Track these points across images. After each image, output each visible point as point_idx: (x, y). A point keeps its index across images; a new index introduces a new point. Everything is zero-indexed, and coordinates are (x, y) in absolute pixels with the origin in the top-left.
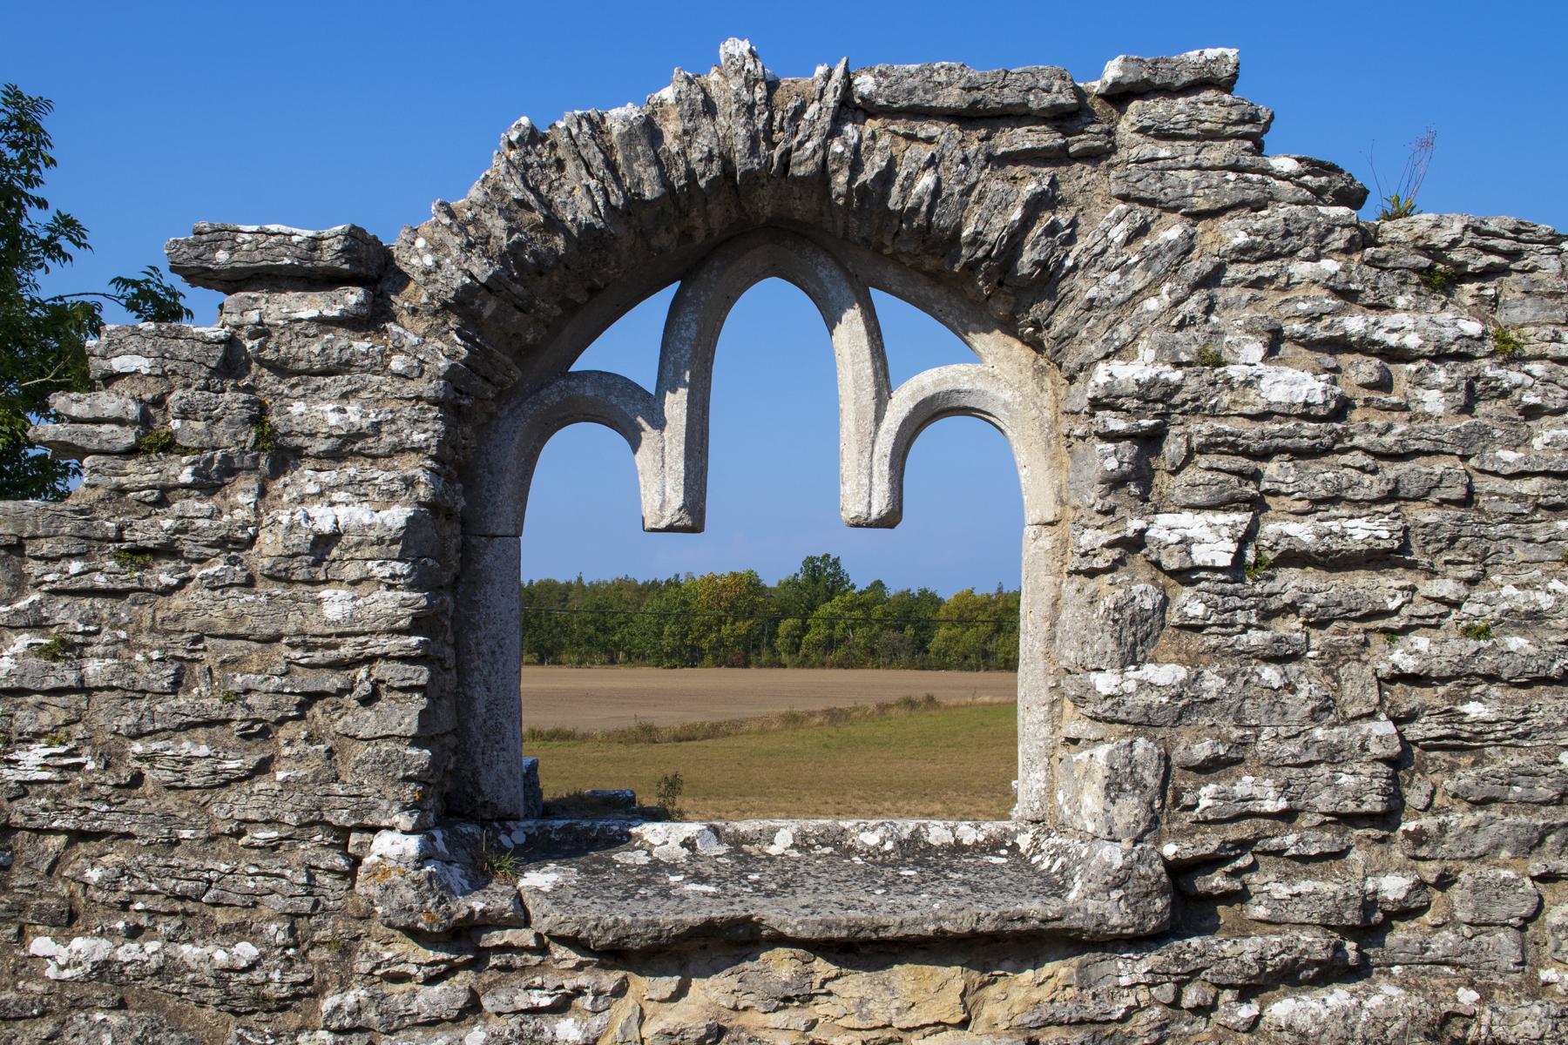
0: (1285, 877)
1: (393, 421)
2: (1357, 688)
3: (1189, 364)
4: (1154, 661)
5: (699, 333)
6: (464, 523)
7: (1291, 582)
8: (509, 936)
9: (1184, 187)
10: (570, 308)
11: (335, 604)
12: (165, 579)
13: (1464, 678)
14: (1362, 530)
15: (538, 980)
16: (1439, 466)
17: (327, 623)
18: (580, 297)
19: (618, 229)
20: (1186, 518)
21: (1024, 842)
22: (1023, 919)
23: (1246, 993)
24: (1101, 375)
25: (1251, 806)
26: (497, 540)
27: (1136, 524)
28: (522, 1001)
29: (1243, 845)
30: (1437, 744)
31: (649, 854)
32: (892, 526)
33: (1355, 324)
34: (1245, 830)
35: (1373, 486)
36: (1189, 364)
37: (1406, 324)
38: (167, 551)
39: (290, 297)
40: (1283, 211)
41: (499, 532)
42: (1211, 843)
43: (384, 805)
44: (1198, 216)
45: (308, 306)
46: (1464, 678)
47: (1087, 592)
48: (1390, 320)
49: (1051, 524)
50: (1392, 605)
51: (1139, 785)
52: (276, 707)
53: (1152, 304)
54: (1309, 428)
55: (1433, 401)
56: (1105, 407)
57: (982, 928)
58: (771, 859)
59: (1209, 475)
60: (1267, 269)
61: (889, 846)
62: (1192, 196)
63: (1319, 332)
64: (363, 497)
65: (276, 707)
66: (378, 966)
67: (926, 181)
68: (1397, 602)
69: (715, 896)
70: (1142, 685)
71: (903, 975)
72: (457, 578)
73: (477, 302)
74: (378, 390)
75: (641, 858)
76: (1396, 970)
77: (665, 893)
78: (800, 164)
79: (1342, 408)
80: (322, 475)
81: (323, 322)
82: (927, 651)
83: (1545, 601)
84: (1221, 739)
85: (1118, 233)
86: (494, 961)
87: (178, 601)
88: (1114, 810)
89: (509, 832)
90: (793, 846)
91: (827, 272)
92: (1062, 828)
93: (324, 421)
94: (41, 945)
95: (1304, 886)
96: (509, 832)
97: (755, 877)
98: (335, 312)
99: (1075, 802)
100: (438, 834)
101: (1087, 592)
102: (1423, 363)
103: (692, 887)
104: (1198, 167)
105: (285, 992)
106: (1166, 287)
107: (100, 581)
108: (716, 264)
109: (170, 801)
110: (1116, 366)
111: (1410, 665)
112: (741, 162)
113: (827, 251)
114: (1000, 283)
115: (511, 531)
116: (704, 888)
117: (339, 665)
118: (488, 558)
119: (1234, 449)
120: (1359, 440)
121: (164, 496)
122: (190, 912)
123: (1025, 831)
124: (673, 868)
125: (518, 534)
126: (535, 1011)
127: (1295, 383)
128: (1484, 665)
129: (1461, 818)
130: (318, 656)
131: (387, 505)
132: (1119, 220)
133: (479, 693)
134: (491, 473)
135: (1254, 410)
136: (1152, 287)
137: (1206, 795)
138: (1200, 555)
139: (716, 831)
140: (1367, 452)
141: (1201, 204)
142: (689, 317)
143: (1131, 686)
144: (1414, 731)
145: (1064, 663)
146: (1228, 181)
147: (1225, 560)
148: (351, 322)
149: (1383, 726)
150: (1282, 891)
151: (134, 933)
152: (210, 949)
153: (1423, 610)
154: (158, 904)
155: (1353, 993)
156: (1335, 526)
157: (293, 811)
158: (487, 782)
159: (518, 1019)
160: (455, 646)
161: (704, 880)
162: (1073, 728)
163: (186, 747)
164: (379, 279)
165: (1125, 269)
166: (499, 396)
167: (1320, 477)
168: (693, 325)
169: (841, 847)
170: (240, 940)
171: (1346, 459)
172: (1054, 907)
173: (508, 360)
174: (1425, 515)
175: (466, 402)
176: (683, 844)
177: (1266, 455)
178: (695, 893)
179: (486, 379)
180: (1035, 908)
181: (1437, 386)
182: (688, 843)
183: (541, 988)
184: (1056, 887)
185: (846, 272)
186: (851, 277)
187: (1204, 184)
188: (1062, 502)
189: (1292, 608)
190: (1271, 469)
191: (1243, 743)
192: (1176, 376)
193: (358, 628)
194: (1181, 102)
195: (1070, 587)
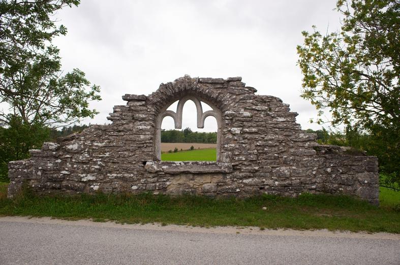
0: (245, 167)
2: (253, 146)
7: (246, 136)
8: (161, 173)
10: (167, 103)
11: (142, 137)
12: (270, 142)
13: (265, 146)
14: (254, 130)
16: (262, 123)
19: (173, 95)
20: (235, 128)
23: (241, 179)
24: (226, 112)
27: (230, 129)
28: (163, 180)
29: (240, 163)
30: (262, 153)
33: (254, 107)
34: (241, 162)
35: (255, 125)
37: (259, 107)
38: (123, 131)
39: (253, 183)
40: (246, 95)
42: (237, 163)
44: (237, 95)
45: (139, 103)
46: (265, 146)
54: (249, 119)
55: (262, 116)
60: (244, 101)
64: (145, 125)
67: (207, 91)
79: (252, 117)
81: (140, 105)
82: (393, 182)
83: (273, 138)
85: (228, 97)
87: (124, 137)
91: (196, 100)
92: (221, 162)
94: (109, 175)
98: (141, 104)
107: (115, 134)
109: (123, 159)
111: (259, 144)
117: (143, 144)
119: (240, 121)
121: (123, 124)
122: (127, 170)
127: (247, 114)
128: (267, 144)
129: (264, 161)
137: (237, 158)
138: (236, 132)
141: (237, 94)
142: (180, 104)
144: (259, 151)
147: (239, 133)
148: (143, 105)
149: (256, 151)
150: (245, 168)
151: (119, 173)
154: (122, 170)
162: (222, 151)
163: (125, 153)
167: (250, 124)
172: (220, 170)
174: (261, 128)
177: (244, 121)
180: (218, 169)
182: (180, 163)
184: (220, 168)
189: (246, 138)
190: (244, 123)
191: (241, 153)
192: (234, 113)
194: (235, 83)
195: (222, 135)
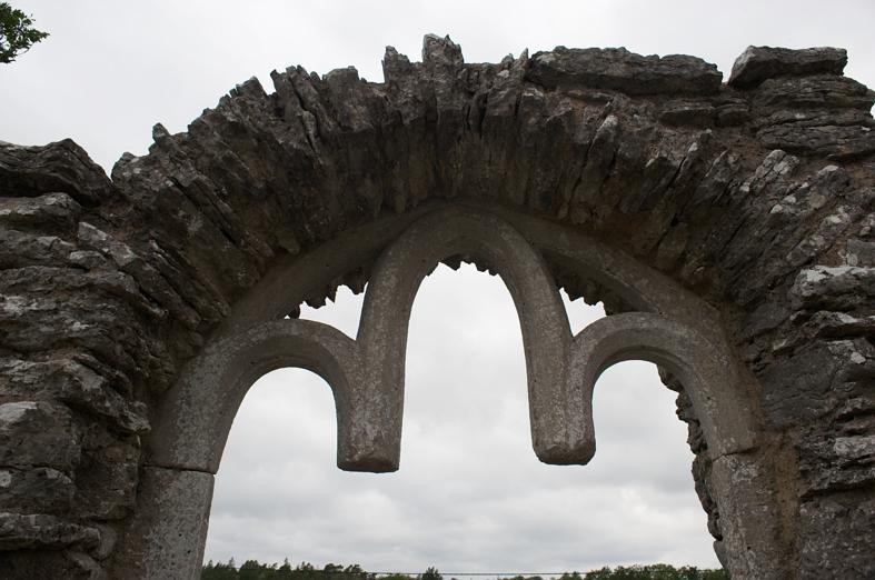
1: (56, 311)
5: (397, 285)
9: (827, 138)
18: (292, 246)
26: (185, 473)
32: (584, 461)
41: (187, 464)
56: (823, 306)
62: (836, 143)
73: (181, 213)
74: (51, 281)
78: (496, 106)
108: (415, 231)
112: (441, 105)
114: (675, 222)
115: (202, 464)
125: (211, 469)
134: (189, 404)
136: (830, 208)
141: (846, 150)
146: (864, 132)
168: (393, 277)
175: (157, 311)
187: (844, 135)
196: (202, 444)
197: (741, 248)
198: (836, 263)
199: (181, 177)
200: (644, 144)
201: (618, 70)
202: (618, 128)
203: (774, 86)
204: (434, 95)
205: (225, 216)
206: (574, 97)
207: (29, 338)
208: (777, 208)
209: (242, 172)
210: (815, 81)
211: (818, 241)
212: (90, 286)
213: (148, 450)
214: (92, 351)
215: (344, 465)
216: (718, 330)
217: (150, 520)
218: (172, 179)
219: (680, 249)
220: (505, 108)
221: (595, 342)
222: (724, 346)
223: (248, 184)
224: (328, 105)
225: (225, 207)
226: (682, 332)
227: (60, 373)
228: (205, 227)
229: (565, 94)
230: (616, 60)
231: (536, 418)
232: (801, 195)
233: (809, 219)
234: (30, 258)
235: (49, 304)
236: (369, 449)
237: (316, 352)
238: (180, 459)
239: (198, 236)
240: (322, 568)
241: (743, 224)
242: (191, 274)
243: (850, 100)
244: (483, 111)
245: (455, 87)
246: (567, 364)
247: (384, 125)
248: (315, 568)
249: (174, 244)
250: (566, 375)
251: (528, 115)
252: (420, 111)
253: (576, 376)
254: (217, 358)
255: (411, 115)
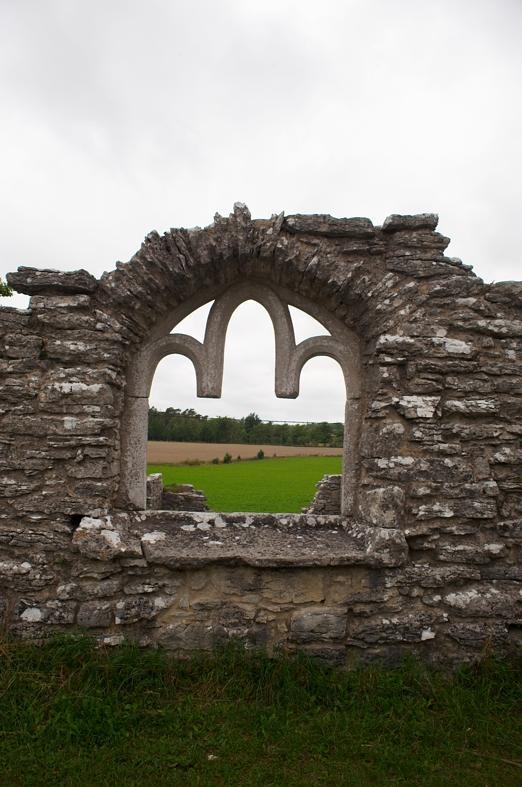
1: (96, 349)
3: (417, 336)
4: (401, 455)
6: (125, 391)
7: (456, 426)
15: (148, 581)
17: (66, 430)
20: (414, 398)
21: (344, 524)
22: (348, 560)
24: (382, 339)
25: (439, 514)
29: (435, 530)
31: (195, 526)
33: (482, 323)
36: (417, 336)
40: (455, 277)
43: (86, 506)
45: (65, 302)
47: (374, 426)
48: (497, 322)
49: (357, 399)
50: (495, 435)
51: (396, 506)
52: (43, 464)
53: (402, 312)
56: (383, 352)
57: (332, 563)
58: (244, 529)
59: (424, 381)
61: (291, 525)
63: (467, 325)
65: (43, 464)
66: (81, 574)
68: (497, 434)
69: (222, 547)
70: (396, 464)
71: (198, 580)
72: (122, 413)
75: (191, 528)
76: (494, 581)
77: (201, 545)
80: (67, 370)
81: (70, 309)
84: (429, 487)
85: (390, 284)
86: (179, 536)
88: (385, 515)
89: (140, 515)
90: (253, 524)
91: (272, 298)
93: (87, 428)
95: (460, 548)
96: (140, 515)
97: (237, 538)
99: (368, 513)
100: (108, 518)
101: (374, 426)
102: (508, 340)
103: (212, 542)
104: (421, 259)
105: (42, 583)
106: (407, 307)
110: (388, 337)
111: (502, 459)
112: (241, 251)
113: (273, 290)
114: (341, 303)
115: (145, 395)
116: (218, 543)
118: (135, 406)
119: (434, 371)
120: (484, 369)
123: (344, 520)
124: (205, 533)
126: (146, 594)
127: (459, 346)
130: (61, 444)
131: (93, 383)
132: (390, 279)
133: (129, 459)
135: (442, 355)
136: (402, 306)
138: (421, 413)
139: (223, 516)
140: (486, 373)
141: (421, 274)
143: (392, 465)
145: (363, 454)
149: (493, 484)
152: (11, 564)
153: (507, 437)
155: (479, 592)
156: (473, 403)
157: (48, 508)
158: (131, 495)
159: (138, 597)
160: (121, 440)
161: (218, 539)
164: (93, 293)
165: (392, 299)
166: (141, 342)
167: (468, 384)
169: (272, 523)
170: (25, 561)
171: (478, 376)
172: (360, 556)
173: (145, 327)
176: (209, 523)
178: (213, 545)
179: (136, 335)
181: (514, 349)
182: (211, 522)
183: (149, 584)
184: (360, 544)
185: (279, 297)
186: (281, 300)
188: (363, 391)
191: (437, 489)
193: (78, 433)
195: (366, 425)
196: (144, 388)
197: (366, 319)
198: (393, 334)
199: (132, 289)
200: (329, 271)
201: (324, 229)
202: (318, 265)
203: (400, 237)
204: (237, 245)
205: (150, 301)
206: (302, 242)
207: (88, 359)
208: (379, 306)
209: (155, 284)
210: (420, 235)
211: (391, 323)
212: (107, 340)
213: (125, 391)
214: (113, 365)
215: (198, 396)
216: (357, 347)
217: (130, 416)
218: (129, 290)
219: (344, 313)
220: (268, 253)
221: (303, 350)
222: (358, 354)
223: (158, 288)
224: (190, 250)
225: (149, 297)
226: (341, 348)
227: (105, 373)
228: (142, 305)
229: (298, 240)
230: (324, 223)
231: (328, 236)
232: (392, 299)
233: (391, 312)
234: (80, 326)
235: (93, 346)
236: (209, 388)
237: (184, 346)
238: (137, 395)
239: (139, 309)
240: (165, 410)
241: (367, 310)
242: (137, 324)
243: (433, 245)
244: (259, 252)
245: (247, 239)
246: (290, 359)
247: (215, 258)
248: (158, 410)
249: (131, 314)
250: (289, 365)
251: (278, 256)
252: (231, 252)
253: (294, 365)
254: (146, 353)
255: (227, 254)
